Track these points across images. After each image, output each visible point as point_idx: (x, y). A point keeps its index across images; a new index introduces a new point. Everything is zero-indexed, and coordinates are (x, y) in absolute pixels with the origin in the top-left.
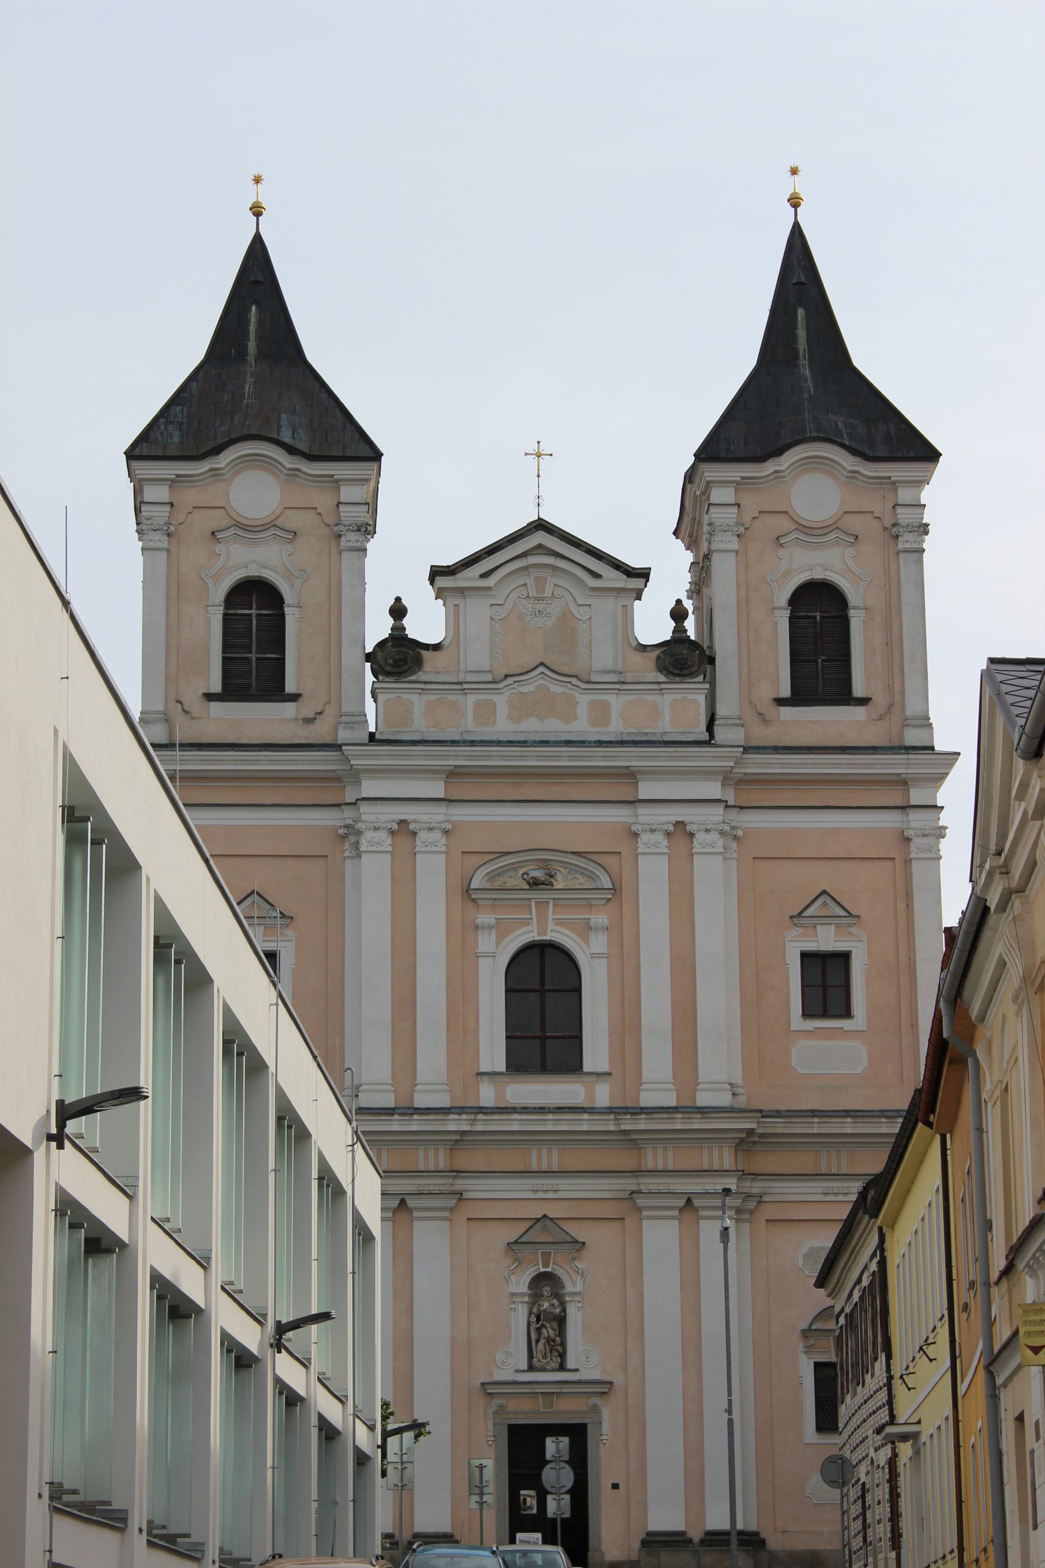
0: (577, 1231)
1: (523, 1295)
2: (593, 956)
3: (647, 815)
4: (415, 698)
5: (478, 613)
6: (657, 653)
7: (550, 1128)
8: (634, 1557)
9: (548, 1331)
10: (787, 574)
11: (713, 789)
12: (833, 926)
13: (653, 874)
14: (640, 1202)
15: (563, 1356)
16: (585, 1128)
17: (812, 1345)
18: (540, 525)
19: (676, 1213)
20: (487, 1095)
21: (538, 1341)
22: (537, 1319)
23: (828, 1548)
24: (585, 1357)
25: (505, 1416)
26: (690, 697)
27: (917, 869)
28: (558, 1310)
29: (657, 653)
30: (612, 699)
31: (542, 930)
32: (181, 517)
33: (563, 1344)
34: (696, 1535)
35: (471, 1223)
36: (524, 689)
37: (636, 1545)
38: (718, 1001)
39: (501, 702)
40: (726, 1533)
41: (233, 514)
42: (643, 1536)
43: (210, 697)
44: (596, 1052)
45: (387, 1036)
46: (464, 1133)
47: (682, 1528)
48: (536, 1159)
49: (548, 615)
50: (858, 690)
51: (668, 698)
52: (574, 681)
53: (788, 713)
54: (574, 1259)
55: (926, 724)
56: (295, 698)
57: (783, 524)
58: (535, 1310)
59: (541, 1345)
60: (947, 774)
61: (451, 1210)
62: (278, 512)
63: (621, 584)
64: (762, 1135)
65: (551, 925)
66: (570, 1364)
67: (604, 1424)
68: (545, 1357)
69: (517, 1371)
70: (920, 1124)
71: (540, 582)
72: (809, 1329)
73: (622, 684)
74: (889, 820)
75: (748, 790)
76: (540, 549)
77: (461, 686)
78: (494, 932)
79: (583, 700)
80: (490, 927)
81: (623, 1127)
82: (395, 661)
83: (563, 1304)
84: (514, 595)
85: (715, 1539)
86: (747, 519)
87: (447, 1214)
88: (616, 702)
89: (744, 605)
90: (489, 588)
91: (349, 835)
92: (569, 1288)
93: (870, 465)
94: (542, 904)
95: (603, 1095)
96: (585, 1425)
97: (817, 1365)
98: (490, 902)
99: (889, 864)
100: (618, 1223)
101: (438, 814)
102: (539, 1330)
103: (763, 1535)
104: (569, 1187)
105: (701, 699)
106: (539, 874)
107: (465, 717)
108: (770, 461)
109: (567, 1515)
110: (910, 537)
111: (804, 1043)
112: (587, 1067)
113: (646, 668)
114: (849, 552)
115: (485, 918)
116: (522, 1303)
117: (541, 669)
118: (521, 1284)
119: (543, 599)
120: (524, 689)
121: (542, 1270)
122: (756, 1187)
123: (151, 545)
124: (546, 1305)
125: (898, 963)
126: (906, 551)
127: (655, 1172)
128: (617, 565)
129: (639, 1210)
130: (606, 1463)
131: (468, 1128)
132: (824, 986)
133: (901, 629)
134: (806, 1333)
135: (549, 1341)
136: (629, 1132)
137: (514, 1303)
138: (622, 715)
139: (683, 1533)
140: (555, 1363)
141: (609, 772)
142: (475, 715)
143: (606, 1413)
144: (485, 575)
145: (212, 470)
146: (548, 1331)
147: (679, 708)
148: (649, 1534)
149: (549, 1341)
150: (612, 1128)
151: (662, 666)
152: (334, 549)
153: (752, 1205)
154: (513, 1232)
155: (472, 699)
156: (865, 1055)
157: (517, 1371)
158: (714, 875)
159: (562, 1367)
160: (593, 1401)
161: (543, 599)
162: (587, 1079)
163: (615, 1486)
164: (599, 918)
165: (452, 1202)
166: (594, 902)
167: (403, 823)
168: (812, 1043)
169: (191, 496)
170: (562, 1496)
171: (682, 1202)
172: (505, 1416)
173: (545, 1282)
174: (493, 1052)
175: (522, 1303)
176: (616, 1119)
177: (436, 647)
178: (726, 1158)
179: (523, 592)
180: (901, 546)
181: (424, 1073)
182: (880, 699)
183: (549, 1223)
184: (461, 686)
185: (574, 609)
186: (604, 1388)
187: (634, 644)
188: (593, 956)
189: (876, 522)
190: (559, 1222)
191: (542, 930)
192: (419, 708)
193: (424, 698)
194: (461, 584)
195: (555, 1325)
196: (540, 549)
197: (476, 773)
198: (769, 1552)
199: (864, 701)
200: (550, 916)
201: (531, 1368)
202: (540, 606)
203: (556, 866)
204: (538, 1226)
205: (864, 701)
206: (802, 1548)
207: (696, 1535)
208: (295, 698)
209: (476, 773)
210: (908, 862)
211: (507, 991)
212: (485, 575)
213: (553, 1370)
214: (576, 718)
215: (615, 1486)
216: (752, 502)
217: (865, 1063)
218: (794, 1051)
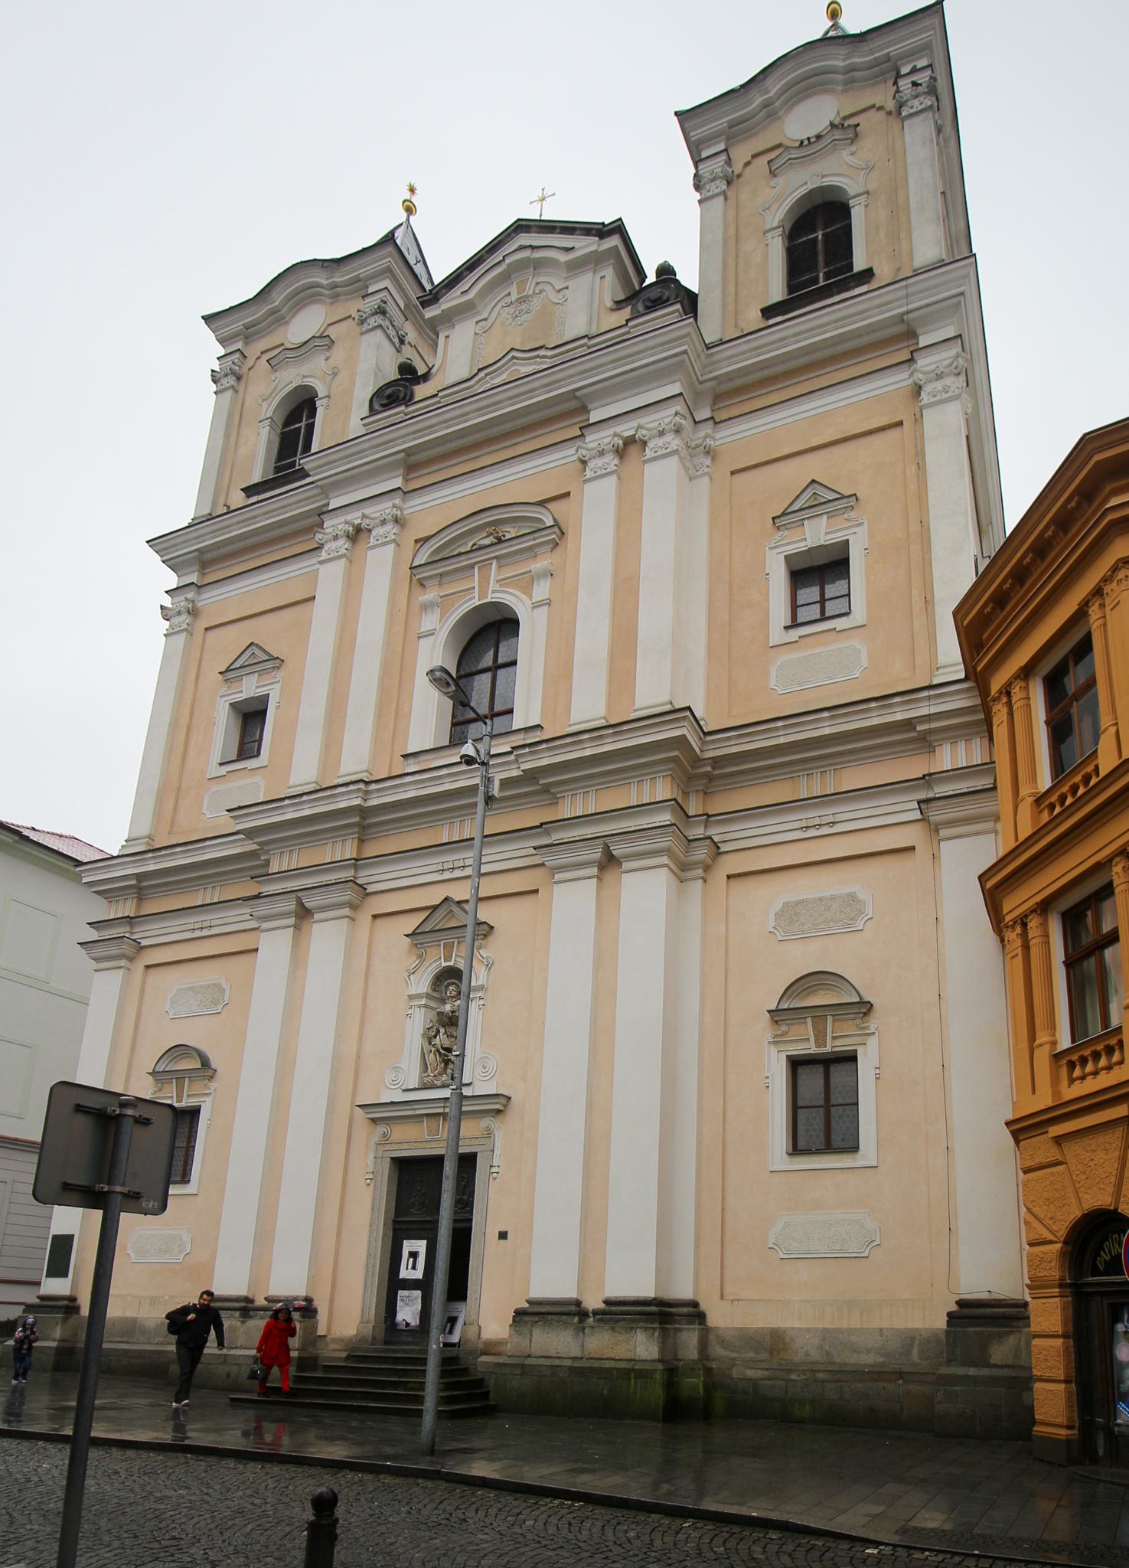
7: (447, 787)
12: (825, 517)
13: (595, 511)
17: (785, 1034)
19: (594, 871)
23: (797, 1325)
25: (388, 1147)
32: (250, 362)
47: (572, 1294)
61: (354, 907)
64: (716, 762)
70: (855, 270)
87: (347, 911)
98: (436, 581)
103: (703, 1307)
116: (420, 1006)
117: (514, 354)
118: (422, 984)
121: (444, 964)
130: (492, 1209)
143: (499, 1137)
152: (935, 842)
154: (412, 923)
156: (864, 656)
160: (485, 1122)
171: (596, 854)
172: (388, 1147)
173: (449, 977)
175: (420, 1006)
186: (498, 1106)
188: (536, 606)
206: (760, 1325)
215: (503, 1235)
217: (865, 663)
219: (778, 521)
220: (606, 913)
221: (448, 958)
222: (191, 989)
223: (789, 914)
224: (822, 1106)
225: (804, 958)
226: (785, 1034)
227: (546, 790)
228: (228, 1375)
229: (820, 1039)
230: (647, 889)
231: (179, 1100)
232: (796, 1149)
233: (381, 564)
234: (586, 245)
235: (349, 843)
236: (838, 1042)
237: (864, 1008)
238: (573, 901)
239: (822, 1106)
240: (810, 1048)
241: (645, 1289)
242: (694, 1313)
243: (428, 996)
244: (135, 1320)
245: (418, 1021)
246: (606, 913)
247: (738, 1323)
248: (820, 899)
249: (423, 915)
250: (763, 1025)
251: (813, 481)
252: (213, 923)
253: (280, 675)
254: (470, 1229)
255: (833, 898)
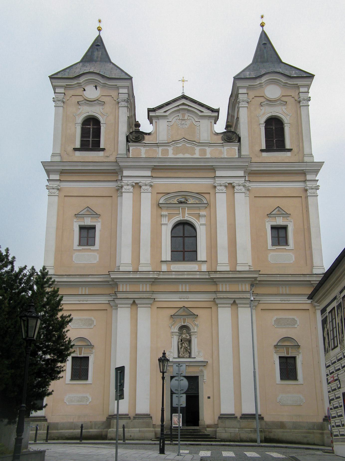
0: (195, 311)
1: (176, 332)
2: (201, 225)
3: (218, 181)
4: (142, 148)
5: (163, 124)
6: (222, 135)
7: (186, 277)
8: (216, 423)
9: (185, 345)
10: (264, 114)
11: (241, 173)
13: (221, 199)
14: (217, 301)
15: (190, 353)
16: (198, 277)
17: (278, 351)
18: (184, 97)
19: (230, 305)
20: (164, 268)
21: (181, 348)
22: (182, 341)
24: (198, 352)
26: (233, 147)
27: (310, 199)
28: (188, 337)
29: (222, 135)
30: (207, 148)
31: (183, 216)
33: (190, 349)
34: (238, 415)
35: (159, 309)
36: (178, 146)
37: (217, 418)
38: (244, 238)
39: (170, 150)
40: (254, 415)
41: (85, 97)
42: (219, 415)
43: (75, 149)
44: (202, 254)
45: (130, 249)
46: (156, 278)
47: (233, 413)
48: (181, 288)
49: (186, 125)
50: (288, 146)
51: (225, 148)
52: (194, 143)
53: (264, 154)
54: (194, 321)
55: (311, 155)
56: (103, 150)
57: (262, 100)
58: (180, 338)
59: (182, 349)
60: (320, 169)
61: (151, 304)
62: (99, 97)
63: (210, 114)
64: (260, 281)
65: (186, 215)
66: (193, 356)
67: (205, 376)
68: (184, 353)
69: (174, 358)
71: (183, 115)
72: (277, 345)
73: (209, 144)
74: (301, 185)
75: (253, 174)
76: (183, 104)
77: (157, 145)
78: (167, 217)
79: (197, 149)
80: (166, 216)
81: (211, 276)
82: (136, 137)
83: (190, 336)
84: (175, 119)
85: (245, 417)
86: (251, 98)
87: (150, 305)
88: (208, 150)
89: (250, 123)
90: (166, 116)
91: (119, 189)
92: (192, 331)
93: (292, 80)
94: (183, 209)
95: (204, 268)
96: (198, 376)
97: (280, 357)
98: (166, 208)
99: (300, 198)
100: (210, 309)
101: (148, 181)
102: (182, 344)
104: (192, 297)
105: (237, 148)
106: (183, 200)
107: (159, 153)
108: (258, 80)
109: (184, 405)
110: (304, 102)
111: (272, 253)
112: (199, 259)
113: (219, 140)
114: (284, 108)
115: (164, 213)
118: (176, 329)
119: (184, 120)
120: (178, 146)
122: (258, 298)
123: (58, 105)
124: (184, 336)
125: (304, 228)
126: (303, 106)
127: (222, 292)
128: (208, 108)
129: (217, 305)
130: (205, 391)
131: (157, 277)
132: (278, 237)
133: (302, 130)
134: (276, 346)
135: (185, 348)
136: (213, 279)
137: (173, 335)
138: (209, 152)
139: (234, 415)
140: (187, 355)
141: (208, 169)
142: (162, 153)
143: (205, 373)
144: (165, 112)
145: (78, 83)
146: (185, 345)
147: (229, 151)
148: (221, 415)
149: (185, 348)
150: (207, 277)
151: (223, 139)
152: (117, 107)
153: (256, 303)
154: (173, 312)
155: (160, 148)
156: (293, 258)
157: (174, 358)
158: (242, 201)
159: (190, 357)
160: (201, 368)
161: (184, 120)
162: (199, 263)
163: (209, 398)
164: (203, 213)
165: (152, 301)
166: (201, 208)
167: (137, 184)
168: (275, 253)
169: (71, 92)
170: (181, 395)
171: (232, 301)
173: (184, 328)
174: (167, 255)
176: (209, 274)
177: (149, 134)
178: (247, 287)
179: (178, 118)
180: (301, 104)
181: (143, 260)
182: (295, 149)
183: (186, 309)
184: (157, 145)
185: (194, 122)
186: (204, 364)
187: (214, 133)
188: (201, 225)
189: (293, 99)
190: (190, 309)
191: (183, 216)
192: (140, 151)
193: (145, 148)
194: (157, 114)
195: (188, 343)
196: (183, 104)
197: (160, 169)
198: (265, 422)
199: (290, 150)
200: (186, 212)
201: (179, 357)
202: (183, 122)
203: (187, 197)
204: (182, 309)
205: (290, 150)
206: (277, 420)
207: (238, 415)
208: (103, 150)
209: (160, 169)
210: (307, 197)
211: (171, 237)
212: (165, 112)
213: (187, 358)
214: (195, 154)
215: (209, 398)
216: (252, 94)
218: (269, 255)
219: (269, 215)
220: (235, 318)
221: (184, 322)
222: (80, 319)
223: (278, 321)
224: (288, 369)
225: (284, 332)
226: (278, 351)
227: (215, 282)
228: (131, 436)
229: (288, 353)
230: (245, 313)
231: (80, 354)
232: (282, 379)
233: (147, 200)
234: (207, 113)
235: (148, 285)
236: (292, 354)
237: (298, 346)
238: (225, 314)
239: (288, 369)
240: (285, 355)
241: (252, 411)
242: (261, 418)
243: (178, 333)
244: (73, 422)
245: (175, 340)
246: (235, 318)
247: (272, 420)
248: (286, 318)
249: (177, 310)
250: (272, 348)
251: (278, 207)
252: (88, 300)
253: (100, 220)
254: (198, 396)
255: (289, 319)
